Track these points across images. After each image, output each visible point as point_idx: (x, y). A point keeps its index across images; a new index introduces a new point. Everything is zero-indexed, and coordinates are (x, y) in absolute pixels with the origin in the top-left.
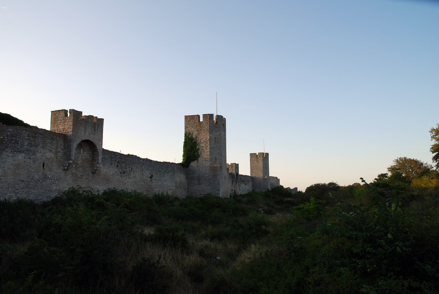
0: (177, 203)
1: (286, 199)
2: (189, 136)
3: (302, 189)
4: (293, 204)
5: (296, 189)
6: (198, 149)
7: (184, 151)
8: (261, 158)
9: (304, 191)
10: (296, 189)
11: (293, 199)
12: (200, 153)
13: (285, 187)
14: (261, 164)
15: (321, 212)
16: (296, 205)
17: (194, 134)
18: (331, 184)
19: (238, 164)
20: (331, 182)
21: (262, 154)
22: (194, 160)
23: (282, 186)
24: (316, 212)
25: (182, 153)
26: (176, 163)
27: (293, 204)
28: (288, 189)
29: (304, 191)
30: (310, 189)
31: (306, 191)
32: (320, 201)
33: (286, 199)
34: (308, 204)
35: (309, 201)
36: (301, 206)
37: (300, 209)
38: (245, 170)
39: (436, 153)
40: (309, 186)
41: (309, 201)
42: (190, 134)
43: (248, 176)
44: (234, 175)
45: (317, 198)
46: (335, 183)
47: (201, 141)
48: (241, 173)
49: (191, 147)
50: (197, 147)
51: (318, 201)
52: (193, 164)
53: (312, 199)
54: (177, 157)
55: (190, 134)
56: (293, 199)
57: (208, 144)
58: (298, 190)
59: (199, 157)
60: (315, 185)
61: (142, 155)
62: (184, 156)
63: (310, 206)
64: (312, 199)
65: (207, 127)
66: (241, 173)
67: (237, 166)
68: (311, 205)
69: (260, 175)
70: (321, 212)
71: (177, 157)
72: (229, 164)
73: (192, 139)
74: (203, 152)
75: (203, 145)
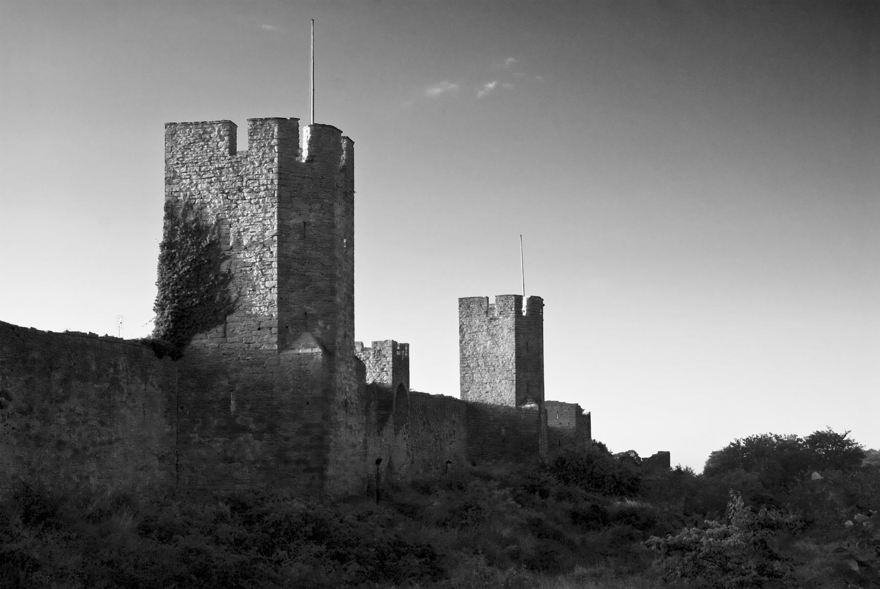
0: (126, 522)
1: (617, 504)
2: (185, 215)
3: (692, 457)
4: (646, 525)
5: (663, 458)
6: (228, 277)
7: (163, 285)
8: (508, 322)
9: (698, 469)
10: (663, 458)
11: (648, 505)
12: (234, 296)
13: (615, 448)
14: (506, 348)
15: (777, 565)
16: (663, 532)
17: (209, 210)
18: (819, 439)
19: (405, 347)
20: (823, 429)
21: (512, 302)
22: (205, 327)
23: (602, 447)
24: (752, 564)
25: (153, 293)
26: (126, 337)
27: (646, 525)
28: (629, 458)
29: (698, 469)
30: (728, 461)
31: (707, 470)
32: (774, 516)
33: (617, 504)
34: (716, 527)
35: (721, 511)
36: (688, 534)
37: (681, 548)
38: (435, 374)
39: (305, 154)
40: (721, 445)
41: (721, 511)
42: (189, 206)
43: (450, 398)
44: (393, 401)
45: (756, 501)
46: (840, 432)
47: (239, 242)
48: (418, 383)
49: (194, 268)
50: (224, 267)
51: (761, 514)
52: (206, 342)
53: (737, 503)
54: (130, 311)
55: (189, 206)
56: (648, 505)
57: (272, 255)
58: (673, 465)
59: (231, 312)
60: (748, 441)
61: (327, 124)
62: (160, 307)
63: (726, 535)
64: (737, 503)
65: (267, 175)
66: (418, 383)
67: (400, 357)
68: (729, 532)
69: (500, 392)
70: (777, 565)
71: (130, 311)
72: (368, 344)
73: (200, 231)
74: (248, 291)
75: (249, 257)
